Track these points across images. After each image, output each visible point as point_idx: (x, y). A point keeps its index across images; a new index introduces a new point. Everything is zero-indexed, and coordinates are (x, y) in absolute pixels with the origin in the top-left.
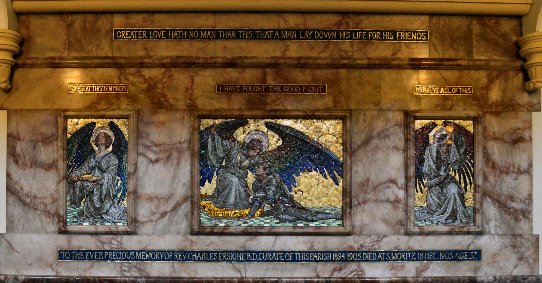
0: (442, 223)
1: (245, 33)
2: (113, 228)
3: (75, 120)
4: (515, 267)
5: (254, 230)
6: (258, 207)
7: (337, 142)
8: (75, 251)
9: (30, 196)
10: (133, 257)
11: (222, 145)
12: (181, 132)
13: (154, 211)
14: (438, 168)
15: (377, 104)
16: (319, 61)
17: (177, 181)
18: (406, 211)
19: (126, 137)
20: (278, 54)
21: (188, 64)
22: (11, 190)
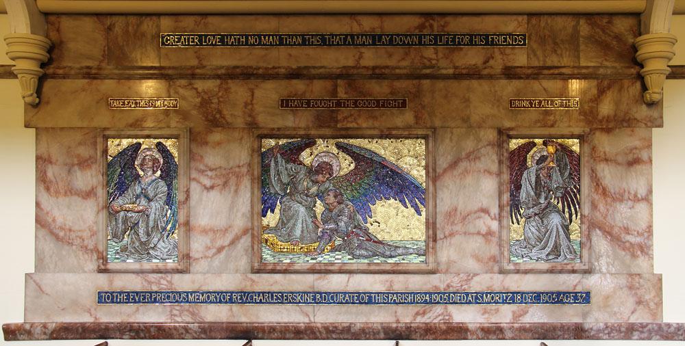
0: (542, 259)
1: (312, 38)
2: (161, 266)
3: (117, 141)
4: (633, 313)
5: (323, 268)
6: (328, 240)
7: (419, 166)
8: (117, 292)
9: (64, 229)
10: (185, 299)
11: (286, 169)
12: (241, 154)
13: (209, 245)
14: (538, 195)
15: (465, 120)
16: (397, 71)
17: (235, 210)
18: (500, 246)
19: (176, 160)
20: (350, 63)
21: (246, 75)
22: (40, 222)
